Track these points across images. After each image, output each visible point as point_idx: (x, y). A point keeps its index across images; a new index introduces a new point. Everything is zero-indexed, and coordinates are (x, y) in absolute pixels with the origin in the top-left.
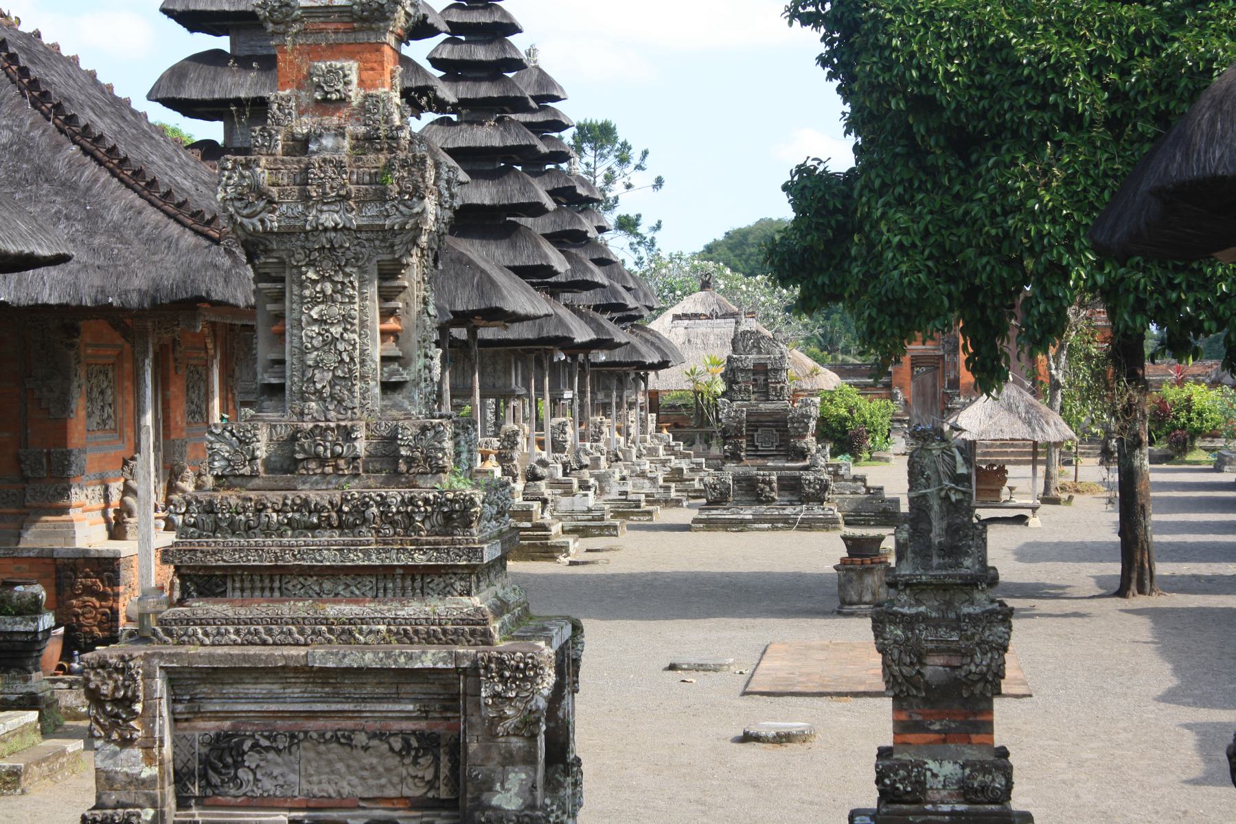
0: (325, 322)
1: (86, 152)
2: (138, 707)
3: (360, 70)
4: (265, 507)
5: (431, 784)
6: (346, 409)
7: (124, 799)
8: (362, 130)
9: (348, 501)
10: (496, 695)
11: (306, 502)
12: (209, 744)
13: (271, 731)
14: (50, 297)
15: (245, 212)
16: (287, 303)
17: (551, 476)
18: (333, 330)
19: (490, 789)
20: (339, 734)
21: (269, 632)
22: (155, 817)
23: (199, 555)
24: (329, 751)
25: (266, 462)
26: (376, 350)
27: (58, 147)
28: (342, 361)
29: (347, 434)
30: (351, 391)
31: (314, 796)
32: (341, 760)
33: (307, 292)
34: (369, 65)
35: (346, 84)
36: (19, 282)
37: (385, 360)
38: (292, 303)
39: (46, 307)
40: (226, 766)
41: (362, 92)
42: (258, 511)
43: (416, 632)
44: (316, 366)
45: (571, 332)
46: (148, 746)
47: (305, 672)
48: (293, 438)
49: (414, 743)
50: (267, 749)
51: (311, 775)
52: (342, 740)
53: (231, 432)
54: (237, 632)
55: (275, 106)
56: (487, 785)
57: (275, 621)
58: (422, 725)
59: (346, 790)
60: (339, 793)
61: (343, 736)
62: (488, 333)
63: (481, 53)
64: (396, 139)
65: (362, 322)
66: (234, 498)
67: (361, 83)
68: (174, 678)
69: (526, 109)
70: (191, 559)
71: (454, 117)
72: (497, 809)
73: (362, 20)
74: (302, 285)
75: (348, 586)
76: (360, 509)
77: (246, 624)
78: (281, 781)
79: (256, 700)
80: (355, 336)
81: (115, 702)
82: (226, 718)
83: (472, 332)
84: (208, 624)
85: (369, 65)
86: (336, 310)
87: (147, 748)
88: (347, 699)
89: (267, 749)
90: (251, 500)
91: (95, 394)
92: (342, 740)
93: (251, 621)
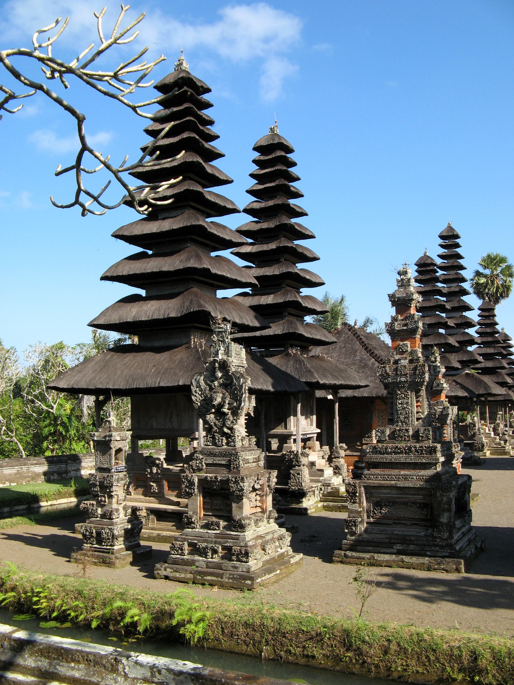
1: (376, 360)
2: (357, 494)
3: (410, 344)
5: (426, 515)
8: (411, 358)
10: (441, 495)
14: (366, 395)
17: (508, 434)
19: (440, 517)
25: (388, 436)
26: (415, 410)
27: (370, 360)
28: (406, 413)
29: (407, 430)
30: (409, 420)
36: (359, 391)
37: (417, 413)
39: (365, 397)
43: (423, 478)
45: (511, 397)
46: (360, 503)
48: (395, 431)
49: (422, 505)
56: (439, 516)
57: (389, 475)
58: (424, 501)
59: (406, 516)
62: (489, 399)
63: (488, 330)
64: (419, 360)
65: (411, 404)
66: (380, 445)
67: (411, 347)
68: (367, 488)
69: (500, 343)
71: (482, 346)
72: (442, 522)
73: (410, 332)
76: (410, 448)
79: (385, 494)
81: (352, 493)
83: (486, 398)
87: (360, 504)
88: (406, 494)
91: (380, 417)
93: (384, 475)
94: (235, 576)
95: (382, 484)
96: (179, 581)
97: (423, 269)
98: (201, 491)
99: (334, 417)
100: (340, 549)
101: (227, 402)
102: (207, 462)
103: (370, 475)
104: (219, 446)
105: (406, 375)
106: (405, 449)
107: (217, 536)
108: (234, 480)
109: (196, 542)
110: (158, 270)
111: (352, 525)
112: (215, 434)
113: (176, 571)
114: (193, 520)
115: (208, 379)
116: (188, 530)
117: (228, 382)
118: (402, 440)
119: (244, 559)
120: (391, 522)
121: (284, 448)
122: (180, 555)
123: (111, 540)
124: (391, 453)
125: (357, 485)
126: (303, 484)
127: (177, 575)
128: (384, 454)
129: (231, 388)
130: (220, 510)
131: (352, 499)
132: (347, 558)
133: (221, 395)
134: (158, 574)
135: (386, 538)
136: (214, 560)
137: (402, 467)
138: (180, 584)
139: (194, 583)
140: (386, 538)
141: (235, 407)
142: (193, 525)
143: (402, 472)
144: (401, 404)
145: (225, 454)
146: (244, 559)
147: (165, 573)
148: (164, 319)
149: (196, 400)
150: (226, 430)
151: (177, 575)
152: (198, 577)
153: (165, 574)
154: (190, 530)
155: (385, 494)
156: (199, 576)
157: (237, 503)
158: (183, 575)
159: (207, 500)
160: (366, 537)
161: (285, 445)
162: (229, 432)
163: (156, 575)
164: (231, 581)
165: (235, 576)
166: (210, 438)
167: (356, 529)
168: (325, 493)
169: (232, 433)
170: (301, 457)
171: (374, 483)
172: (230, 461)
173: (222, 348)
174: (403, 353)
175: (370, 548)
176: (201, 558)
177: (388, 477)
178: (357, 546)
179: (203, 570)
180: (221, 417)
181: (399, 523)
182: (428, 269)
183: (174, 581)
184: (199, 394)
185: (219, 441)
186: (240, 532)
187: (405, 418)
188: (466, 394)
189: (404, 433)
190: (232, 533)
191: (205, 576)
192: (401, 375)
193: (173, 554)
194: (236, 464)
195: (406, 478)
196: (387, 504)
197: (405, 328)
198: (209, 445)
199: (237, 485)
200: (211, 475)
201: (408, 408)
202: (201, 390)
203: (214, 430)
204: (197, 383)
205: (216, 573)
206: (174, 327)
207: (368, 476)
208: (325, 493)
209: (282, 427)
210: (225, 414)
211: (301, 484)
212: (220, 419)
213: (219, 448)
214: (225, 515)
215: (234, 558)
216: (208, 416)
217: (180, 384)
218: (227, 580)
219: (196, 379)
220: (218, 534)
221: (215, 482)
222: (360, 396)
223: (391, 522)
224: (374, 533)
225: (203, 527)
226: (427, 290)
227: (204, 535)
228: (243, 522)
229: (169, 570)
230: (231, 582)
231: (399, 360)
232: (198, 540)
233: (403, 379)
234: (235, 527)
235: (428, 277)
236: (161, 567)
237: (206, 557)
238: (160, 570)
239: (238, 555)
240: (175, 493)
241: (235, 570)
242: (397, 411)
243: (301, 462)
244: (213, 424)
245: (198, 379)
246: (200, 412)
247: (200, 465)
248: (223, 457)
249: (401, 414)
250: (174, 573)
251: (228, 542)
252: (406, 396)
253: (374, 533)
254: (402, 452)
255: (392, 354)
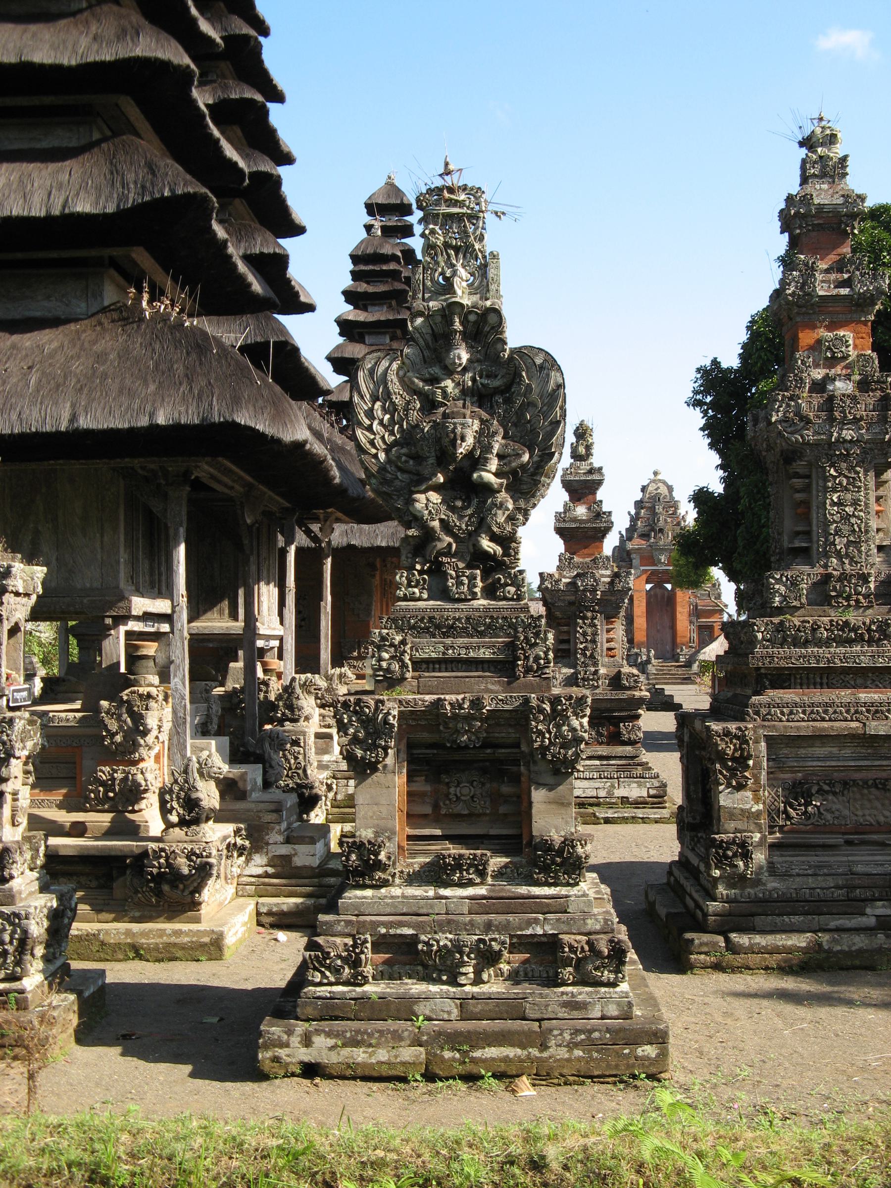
0: (842, 504)
4: (819, 627)
6: (856, 563)
7: (740, 827)
9: (874, 623)
11: (846, 623)
12: (788, 789)
13: (831, 780)
15: (789, 430)
16: (814, 492)
18: (847, 509)
20: (877, 781)
21: (826, 712)
22: (761, 839)
23: (776, 659)
24: (870, 793)
30: (860, 552)
31: (861, 824)
32: (877, 799)
33: (830, 484)
34: (860, 335)
35: (847, 347)
38: (818, 491)
39: (379, 548)
40: (800, 805)
41: (856, 353)
42: (814, 630)
44: (836, 534)
47: (859, 738)
50: (827, 792)
51: (857, 810)
52: (880, 786)
53: (787, 577)
54: (804, 712)
55: (800, 362)
57: (827, 705)
60: (878, 823)
61: (880, 783)
67: (855, 347)
70: (770, 663)
73: (858, 305)
74: (826, 480)
75: (874, 681)
77: (809, 707)
78: (837, 813)
79: (818, 759)
80: (862, 514)
81: (733, 759)
82: (799, 771)
84: (784, 707)
85: (860, 335)
86: (849, 496)
89: (827, 792)
90: (809, 622)
92: (880, 786)
93: (812, 705)
94: (596, 1035)
95: (824, 729)
96: (366, 1078)
97: (371, 267)
98: (403, 755)
99: (320, 597)
100: (702, 928)
101: (496, 447)
102: (419, 655)
103: (769, 705)
104: (459, 600)
105: (856, 420)
106: (869, 630)
107: (478, 905)
108: (547, 707)
109: (410, 932)
110: (13, 59)
111: (735, 855)
112: (445, 560)
113: (355, 1043)
114: (382, 856)
115: (418, 372)
116: (359, 893)
117: (496, 383)
118: (849, 606)
119: (607, 975)
120: (839, 840)
121: (230, 672)
122: (346, 983)
123: (10, 959)
124: (827, 643)
125: (749, 734)
126: (309, 772)
127: (360, 1055)
128: (806, 644)
129: (508, 401)
130: (471, 817)
131: (733, 776)
132: (735, 952)
133: (476, 425)
134: (276, 1059)
135: (837, 887)
136: (484, 988)
137: (859, 681)
138: (375, 1086)
139: (430, 1077)
140: (837, 887)
141: (523, 466)
142: (379, 875)
143: (864, 696)
144: (840, 504)
145: (489, 626)
146: (607, 975)
147: (305, 1055)
148: (49, 220)
149: (372, 443)
150: (486, 544)
151: (360, 1055)
152: (447, 1054)
153: (306, 1059)
154: (369, 893)
155: (818, 759)
156: (453, 1049)
157: (551, 788)
158: (382, 1055)
159: (421, 786)
160: (775, 889)
161: (232, 665)
162: (499, 550)
163: (267, 1066)
164: (578, 1053)
165: (596, 1035)
166: (421, 572)
167: (746, 866)
168: (339, 797)
169: (506, 553)
170: (301, 696)
171: (798, 728)
172: (511, 647)
173: (462, 272)
174: (832, 361)
175: (795, 919)
176: (434, 988)
177: (826, 712)
178: (753, 915)
179: (449, 1027)
180: (468, 501)
181: (863, 843)
182: (385, 268)
183: (343, 1078)
184: (381, 423)
185: (459, 583)
186: (568, 884)
187: (849, 544)
188: (71, 637)
189: (856, 585)
190: (536, 891)
191: (473, 1047)
192: (843, 423)
193: (320, 984)
194: (537, 658)
195: (877, 712)
196: (826, 788)
197: (844, 291)
198: (420, 599)
199: (558, 726)
200: (452, 698)
201: (858, 518)
202: (392, 409)
203: (440, 546)
204: (377, 385)
205: (518, 1033)
206: (54, 255)
207: (764, 711)
208: (339, 797)
209: (221, 612)
210: (487, 490)
211: (305, 771)
212: (464, 508)
213: (461, 606)
214: (493, 832)
215: (568, 972)
216: (421, 497)
217: (161, 420)
218: (563, 1053)
219: (372, 372)
220: (484, 897)
221: (469, 718)
222: (366, 544)
223: (839, 840)
224: (798, 875)
225: (412, 879)
226: (382, 318)
227: (432, 907)
228: (580, 850)
229: (321, 1042)
230: (579, 1059)
231: (827, 379)
232: (418, 926)
233: (848, 434)
234: (545, 869)
235: (381, 288)
236: (290, 1033)
237: (454, 982)
238: (287, 1045)
239: (579, 965)
240: (58, 795)
241: (576, 1014)
242: (826, 524)
243: (300, 709)
244: (436, 524)
245: (381, 369)
246: (385, 482)
247: (396, 666)
248: (482, 634)
249: (838, 532)
250: (346, 1051)
251: (536, 921)
252: (852, 482)
253: (798, 875)
254: (860, 639)
255: (803, 363)
